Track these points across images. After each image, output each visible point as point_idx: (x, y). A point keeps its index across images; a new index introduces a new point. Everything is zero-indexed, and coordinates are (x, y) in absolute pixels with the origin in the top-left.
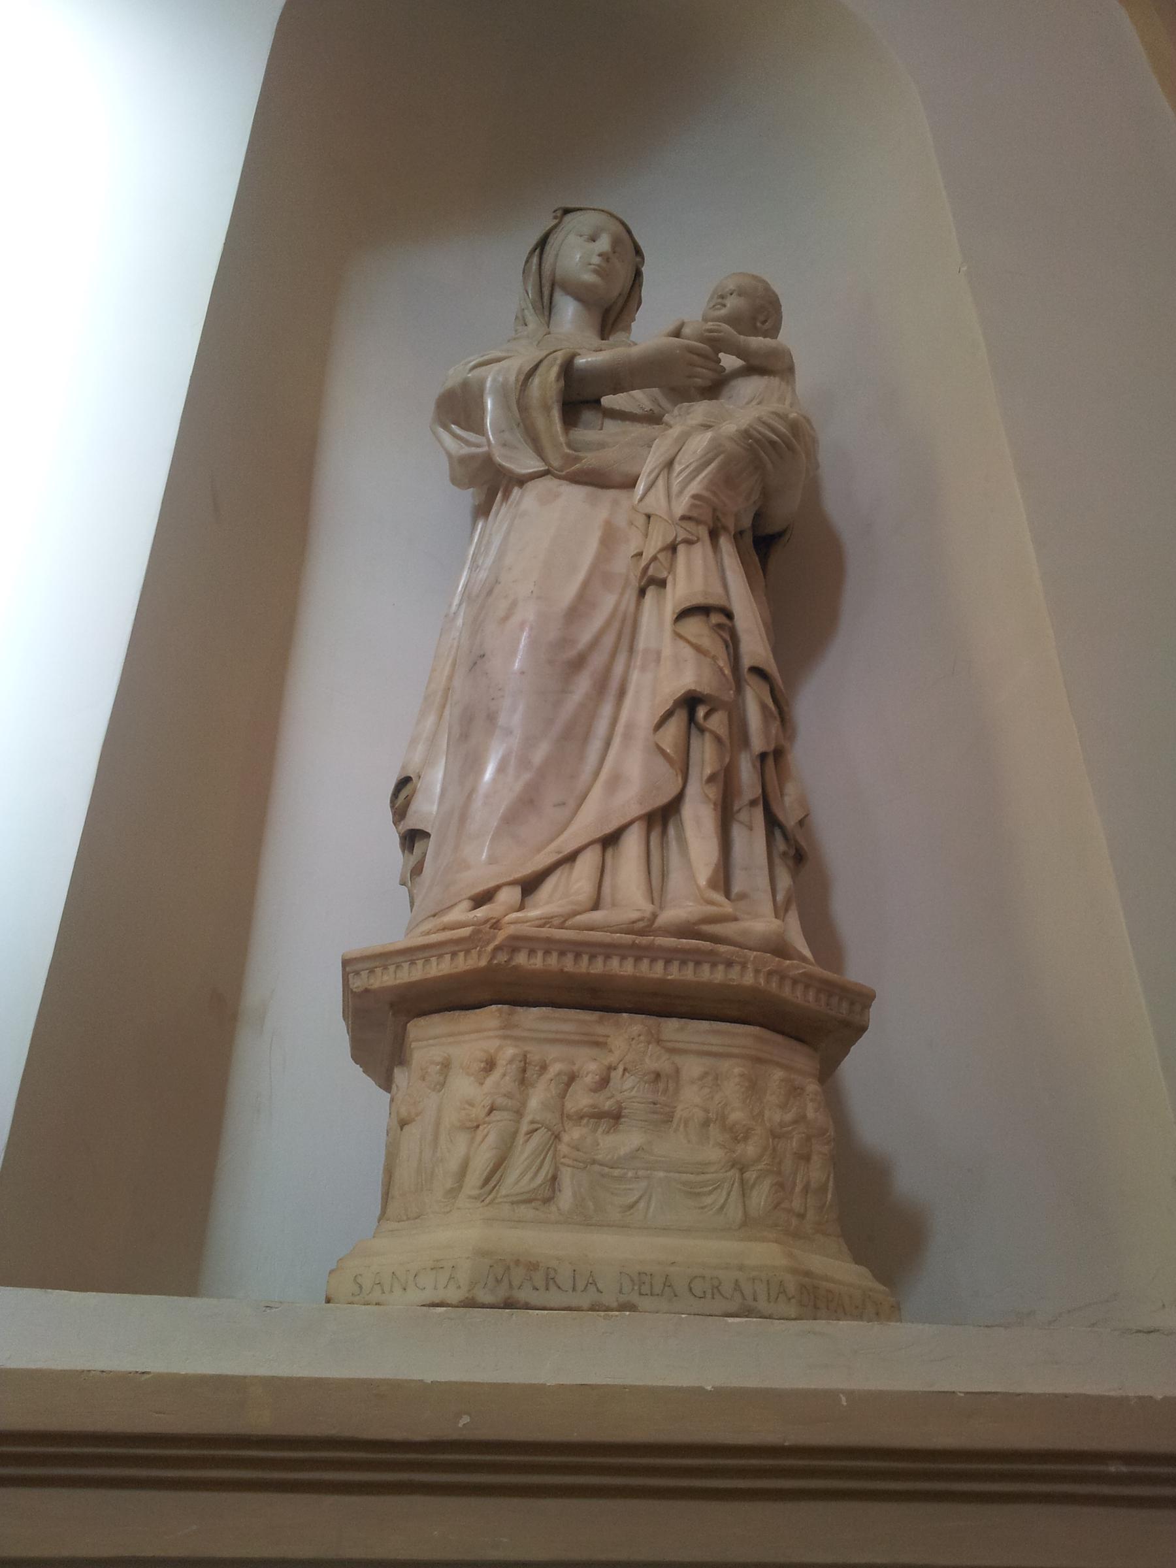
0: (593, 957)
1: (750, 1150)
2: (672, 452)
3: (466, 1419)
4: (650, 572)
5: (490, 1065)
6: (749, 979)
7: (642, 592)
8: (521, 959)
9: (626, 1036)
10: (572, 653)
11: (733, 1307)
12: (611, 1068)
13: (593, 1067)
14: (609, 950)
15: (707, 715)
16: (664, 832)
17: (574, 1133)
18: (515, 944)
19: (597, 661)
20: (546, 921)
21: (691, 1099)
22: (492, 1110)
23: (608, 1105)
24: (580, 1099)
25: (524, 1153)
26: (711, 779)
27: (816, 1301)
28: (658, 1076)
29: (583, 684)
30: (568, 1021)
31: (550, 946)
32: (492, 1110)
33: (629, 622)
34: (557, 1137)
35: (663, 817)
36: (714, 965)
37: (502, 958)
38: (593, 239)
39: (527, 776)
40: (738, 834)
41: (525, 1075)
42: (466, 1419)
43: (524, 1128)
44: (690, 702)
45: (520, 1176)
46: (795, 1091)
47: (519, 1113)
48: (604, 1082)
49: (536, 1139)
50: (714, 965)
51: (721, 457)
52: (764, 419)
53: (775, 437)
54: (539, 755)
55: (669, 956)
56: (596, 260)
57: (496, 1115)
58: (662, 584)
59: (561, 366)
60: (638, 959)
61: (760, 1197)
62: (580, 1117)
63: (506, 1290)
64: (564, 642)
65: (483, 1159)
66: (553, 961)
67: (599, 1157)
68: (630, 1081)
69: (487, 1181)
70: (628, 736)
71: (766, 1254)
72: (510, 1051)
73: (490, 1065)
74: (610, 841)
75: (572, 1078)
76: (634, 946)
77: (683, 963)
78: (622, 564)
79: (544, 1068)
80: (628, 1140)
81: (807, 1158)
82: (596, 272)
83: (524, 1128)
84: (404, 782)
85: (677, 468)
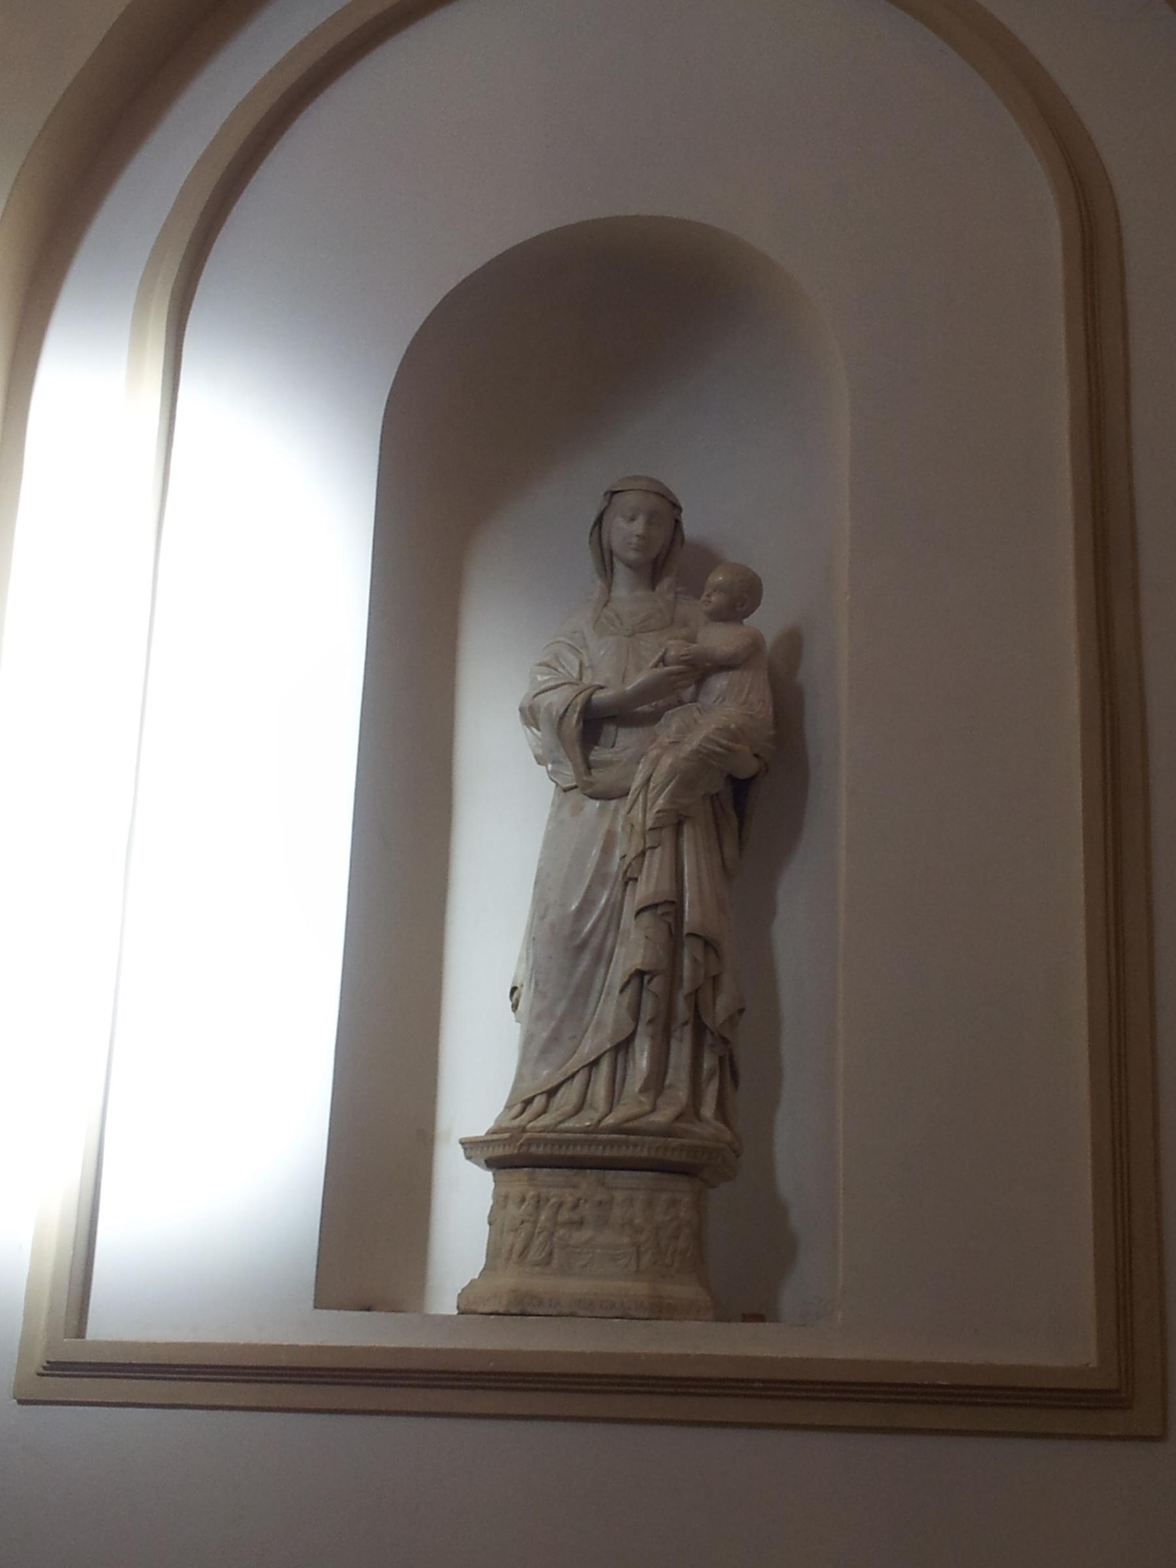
0: (567, 1147)
1: (642, 1238)
2: (648, 773)
3: (491, 1364)
4: (628, 874)
5: (523, 1200)
6: (645, 1154)
7: (626, 884)
8: (533, 1150)
9: (587, 1181)
10: (578, 941)
11: (618, 1314)
12: (580, 1199)
13: (570, 1199)
14: (575, 1142)
15: (650, 981)
16: (627, 1052)
17: (561, 1232)
18: (530, 1142)
19: (595, 941)
20: (545, 1129)
21: (617, 1213)
22: (522, 1222)
23: (576, 1217)
24: (564, 1215)
25: (538, 1240)
26: (650, 1022)
27: (660, 1310)
28: (601, 1203)
29: (586, 958)
30: (560, 1175)
31: (546, 1142)
32: (522, 1222)
33: (617, 906)
34: (552, 1234)
35: (623, 1047)
36: (627, 1147)
37: (524, 1149)
38: (632, 519)
39: (553, 1024)
40: (674, 1045)
41: (539, 1203)
42: (491, 1364)
43: (537, 1230)
44: (640, 974)
45: (534, 1254)
46: (674, 1203)
47: (535, 1222)
48: (576, 1206)
49: (545, 1233)
50: (627, 1147)
51: (677, 778)
52: (712, 736)
53: (718, 749)
54: (560, 1009)
55: (612, 1144)
56: (635, 540)
57: (525, 1224)
58: (636, 880)
59: (580, 712)
60: (590, 1146)
61: (646, 1259)
62: (564, 1224)
63: (522, 1308)
64: (574, 933)
65: (518, 1247)
66: (548, 1150)
67: (571, 1243)
68: (587, 1206)
69: (521, 1254)
70: (608, 994)
71: (639, 1288)
72: (531, 1193)
73: (523, 1200)
74: (595, 1063)
75: (560, 1205)
76: (586, 1140)
77: (612, 1146)
78: (615, 865)
79: (548, 1200)
80: (585, 1234)
81: (677, 1238)
82: (637, 550)
83: (537, 1230)
84: (514, 989)
85: (652, 785)
